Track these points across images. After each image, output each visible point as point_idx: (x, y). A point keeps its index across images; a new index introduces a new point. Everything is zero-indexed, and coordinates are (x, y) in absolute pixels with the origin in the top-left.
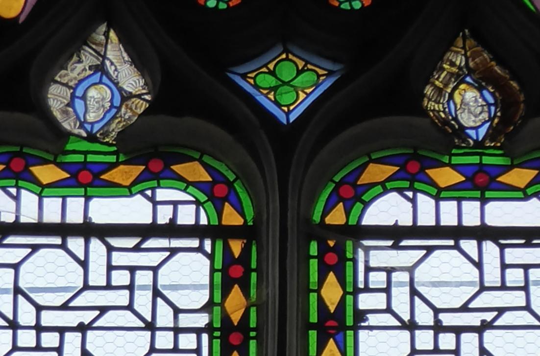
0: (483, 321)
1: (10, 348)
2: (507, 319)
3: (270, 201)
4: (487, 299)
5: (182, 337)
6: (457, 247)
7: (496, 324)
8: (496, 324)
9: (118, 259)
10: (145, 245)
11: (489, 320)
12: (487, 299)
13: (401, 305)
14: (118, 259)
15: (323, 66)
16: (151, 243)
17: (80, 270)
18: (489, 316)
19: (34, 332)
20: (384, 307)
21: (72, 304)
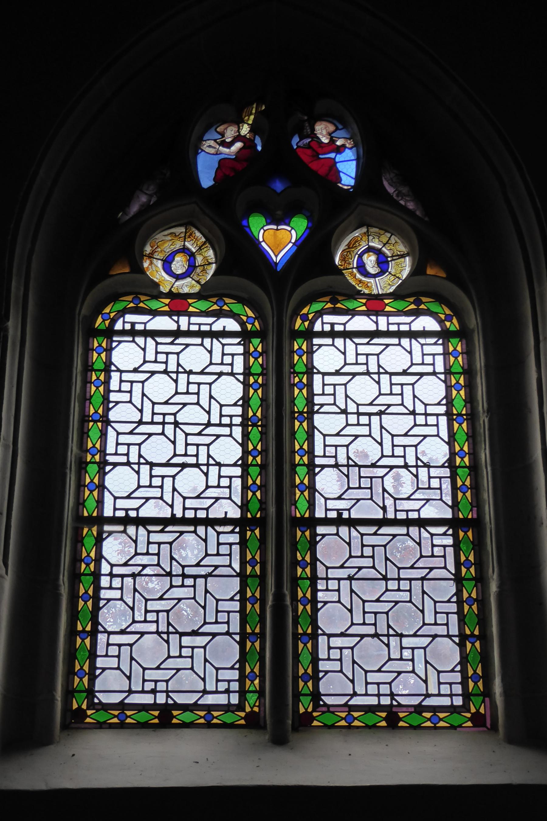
0: (380, 410)
1: (345, 424)
2: (391, 410)
3: (534, 276)
4: (382, 400)
5: (429, 418)
6: (133, 341)
7: (386, 412)
8: (386, 412)
9: (161, 348)
10: (372, 342)
11: (383, 410)
12: (382, 400)
13: (409, 403)
14: (161, 348)
15: (340, 710)
16: (375, 341)
17: (180, 362)
18: (383, 408)
19: (424, 417)
20: (333, 402)
21: (170, 402)
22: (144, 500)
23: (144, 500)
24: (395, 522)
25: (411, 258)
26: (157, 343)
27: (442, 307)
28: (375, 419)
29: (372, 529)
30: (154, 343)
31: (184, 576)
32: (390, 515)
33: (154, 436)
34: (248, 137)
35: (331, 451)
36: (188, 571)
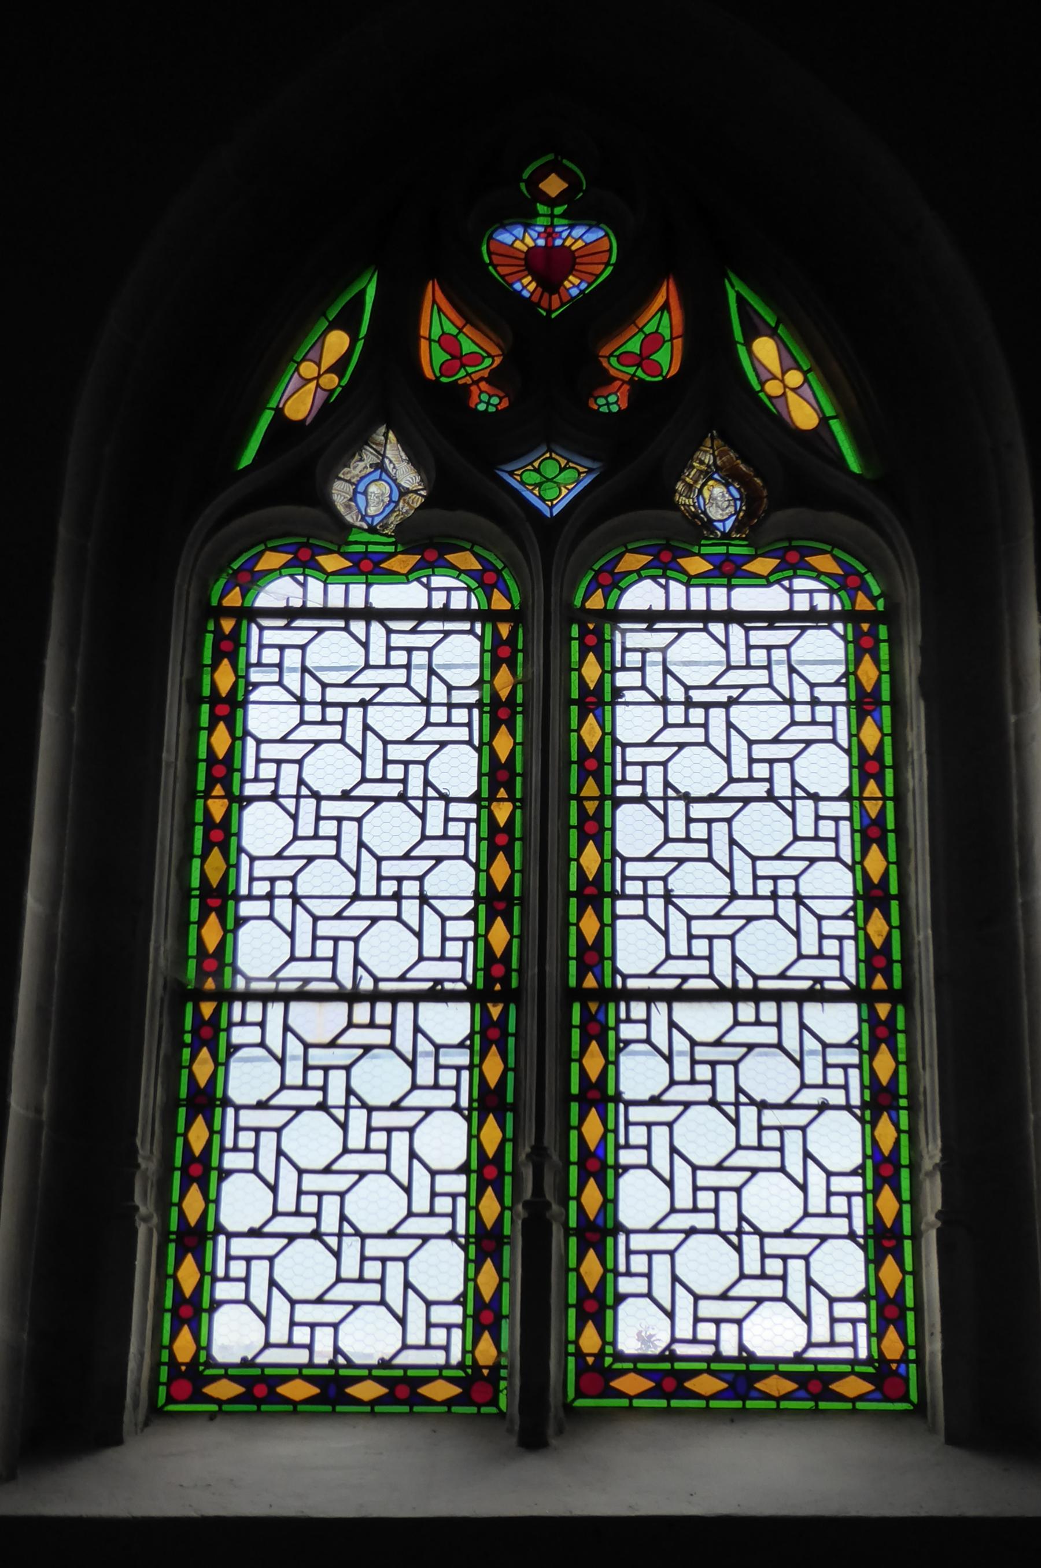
0: (730, 698)
7: (741, 700)
8: (741, 700)
9: (396, 640)
11: (735, 696)
18: (735, 693)
21: (354, 682)
22: (676, 748)
23: (676, 748)
24: (779, 997)
25: (816, 374)
26: (389, 632)
27: (359, 982)
28: (717, 716)
29: (692, 984)
30: (383, 631)
31: (689, 704)
32: (790, 1009)
33: (837, 795)
34: (505, 403)
35: (301, 1335)
36: (697, 696)
